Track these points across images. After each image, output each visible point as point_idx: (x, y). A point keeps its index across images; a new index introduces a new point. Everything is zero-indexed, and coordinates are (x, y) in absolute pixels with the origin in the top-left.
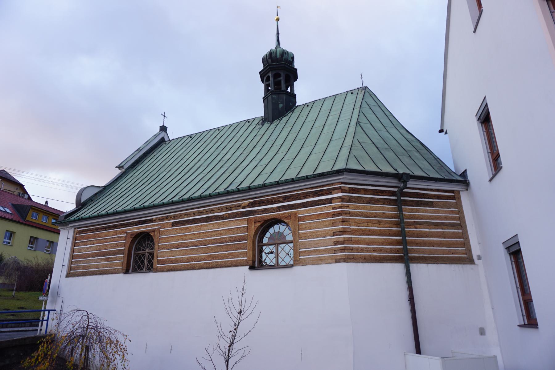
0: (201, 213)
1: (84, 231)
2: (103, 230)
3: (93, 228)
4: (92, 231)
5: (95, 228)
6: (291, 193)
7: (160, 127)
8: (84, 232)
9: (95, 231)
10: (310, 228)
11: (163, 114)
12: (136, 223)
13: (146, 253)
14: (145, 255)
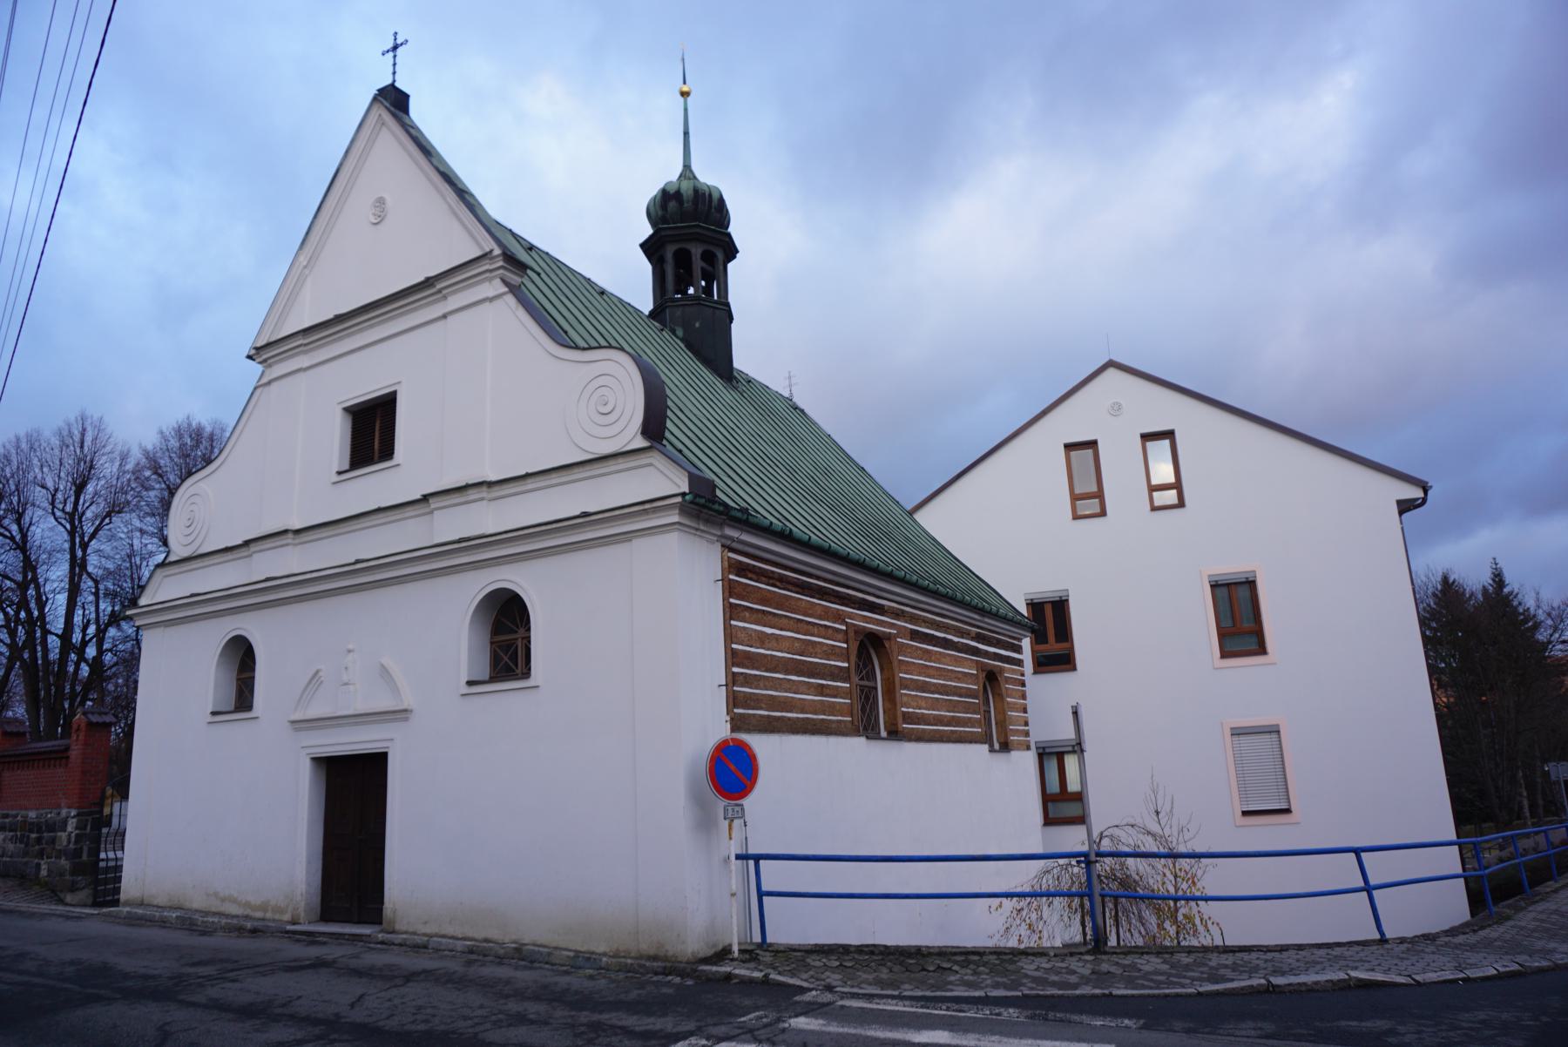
0: (938, 626)
1: (751, 572)
2: (797, 589)
3: (773, 572)
4: (771, 581)
5: (779, 574)
6: (759, 562)
7: (642, 246)
8: (750, 575)
9: (778, 584)
10: (836, 693)
11: (391, 54)
12: (860, 603)
13: (520, 640)
14: (517, 647)
